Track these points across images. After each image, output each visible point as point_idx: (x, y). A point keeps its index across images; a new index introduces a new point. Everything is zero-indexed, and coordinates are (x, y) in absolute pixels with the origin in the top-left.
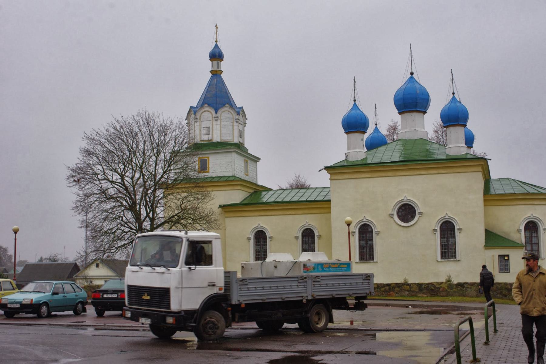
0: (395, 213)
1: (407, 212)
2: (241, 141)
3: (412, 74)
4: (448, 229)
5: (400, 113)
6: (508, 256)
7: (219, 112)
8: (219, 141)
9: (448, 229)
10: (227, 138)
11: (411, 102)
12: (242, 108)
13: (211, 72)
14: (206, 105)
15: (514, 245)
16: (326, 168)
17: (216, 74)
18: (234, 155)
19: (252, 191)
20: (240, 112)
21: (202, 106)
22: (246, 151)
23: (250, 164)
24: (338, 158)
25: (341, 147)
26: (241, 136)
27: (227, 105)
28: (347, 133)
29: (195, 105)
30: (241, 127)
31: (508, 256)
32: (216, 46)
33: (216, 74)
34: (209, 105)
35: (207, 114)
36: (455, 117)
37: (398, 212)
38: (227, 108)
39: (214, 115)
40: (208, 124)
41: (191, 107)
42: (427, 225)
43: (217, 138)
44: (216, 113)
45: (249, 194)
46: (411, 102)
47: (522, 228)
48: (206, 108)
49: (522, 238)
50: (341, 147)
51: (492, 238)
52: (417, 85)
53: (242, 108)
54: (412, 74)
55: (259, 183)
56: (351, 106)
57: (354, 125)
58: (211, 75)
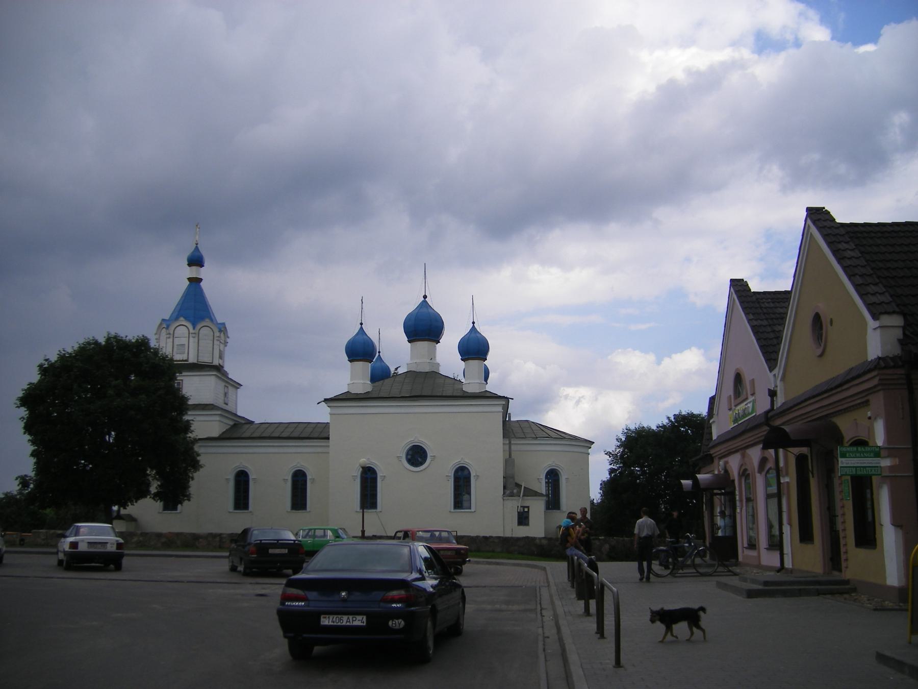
0: (404, 456)
1: (417, 455)
2: (221, 362)
3: (425, 297)
4: (462, 480)
5: (409, 341)
6: (528, 507)
7: (198, 327)
8: (195, 361)
9: (462, 480)
10: (205, 359)
11: (424, 327)
12: (224, 324)
13: (189, 279)
14: (182, 318)
15: (536, 494)
16: (326, 400)
17: (195, 282)
18: (213, 379)
19: (232, 423)
20: (222, 329)
21: (177, 319)
22: (225, 374)
23: (231, 390)
24: (341, 388)
25: (347, 377)
26: (221, 357)
27: (207, 320)
28: (350, 361)
29: (167, 318)
30: (222, 346)
31: (528, 507)
32: (197, 249)
33: (195, 282)
34: (186, 318)
35: (182, 330)
36: (474, 349)
37: (407, 454)
38: (207, 322)
39: (191, 330)
40: (184, 341)
41: (163, 320)
42: (437, 477)
43: (192, 360)
44: (194, 328)
45: (228, 427)
46: (424, 327)
47: (543, 476)
48: (182, 321)
49: (542, 489)
50: (347, 377)
51: (512, 486)
52: (430, 310)
53: (224, 324)
54: (425, 297)
55: (239, 414)
56: (357, 331)
57: (361, 350)
58: (188, 283)
